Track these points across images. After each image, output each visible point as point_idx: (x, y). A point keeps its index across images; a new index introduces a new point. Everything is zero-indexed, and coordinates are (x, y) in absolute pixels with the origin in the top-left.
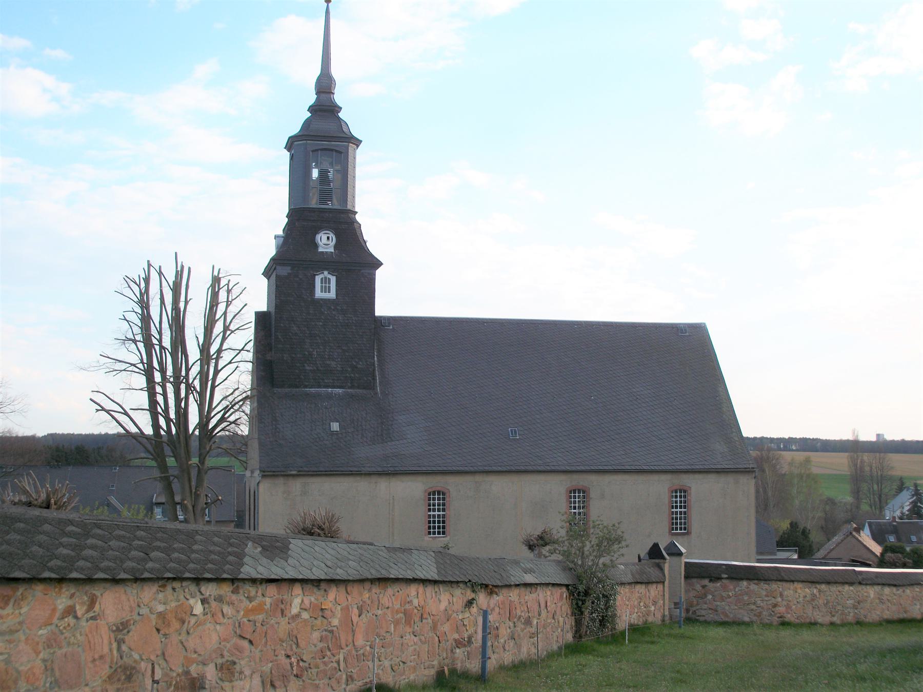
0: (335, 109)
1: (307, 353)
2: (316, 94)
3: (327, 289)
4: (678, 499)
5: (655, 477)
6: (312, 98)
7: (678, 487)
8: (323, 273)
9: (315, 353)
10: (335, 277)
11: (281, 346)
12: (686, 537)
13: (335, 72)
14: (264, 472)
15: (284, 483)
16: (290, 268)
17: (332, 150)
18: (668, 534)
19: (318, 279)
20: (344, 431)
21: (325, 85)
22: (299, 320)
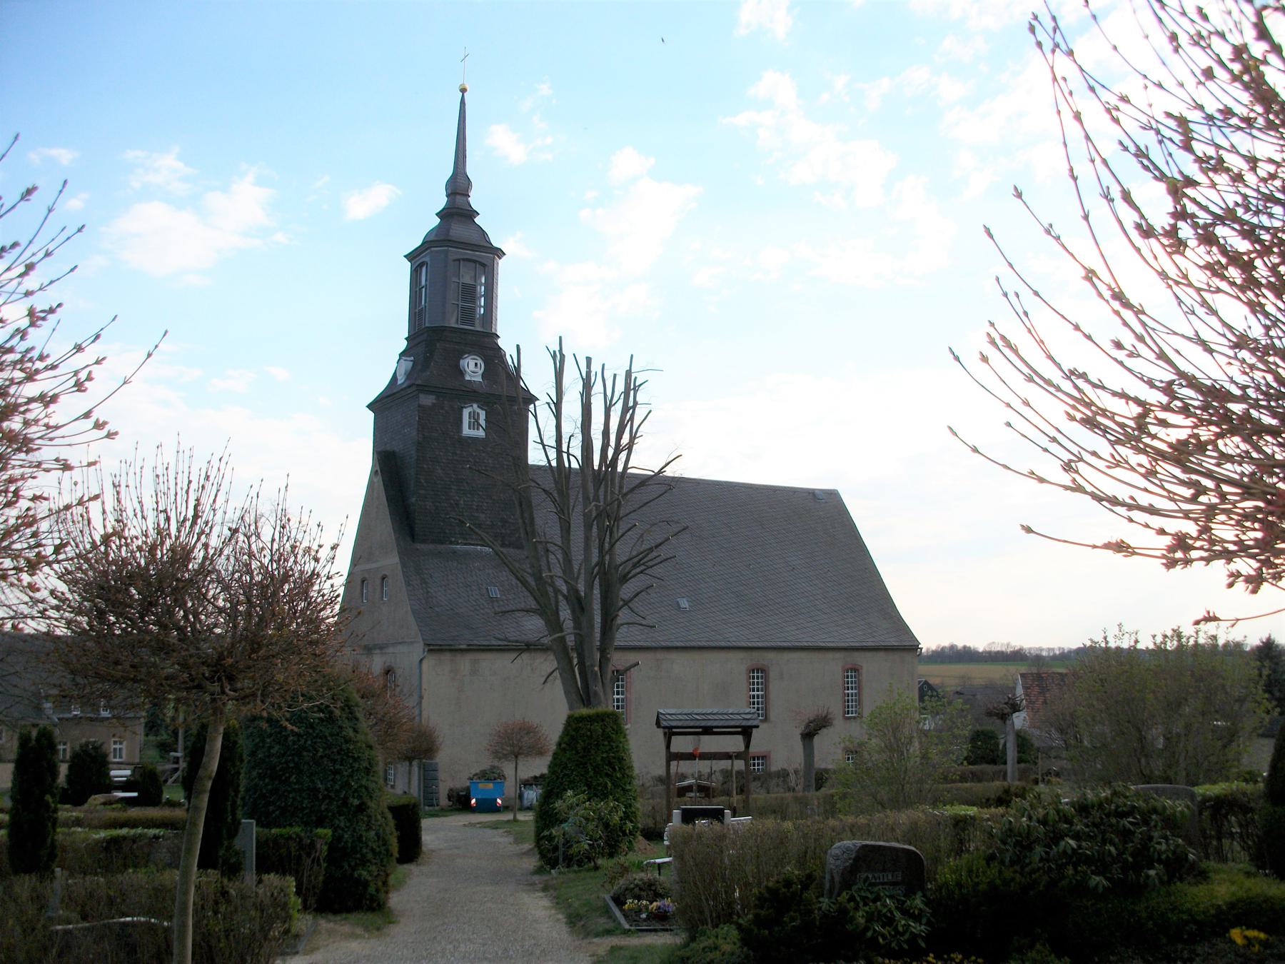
0: (471, 214)
2: (447, 196)
3: (475, 424)
4: (756, 680)
5: (830, 655)
6: (441, 201)
7: (850, 666)
8: (472, 406)
9: (462, 502)
10: (484, 412)
11: (422, 492)
14: (429, 645)
16: (434, 397)
17: (475, 261)
18: (841, 718)
19: (466, 413)
20: (504, 597)
21: (458, 187)
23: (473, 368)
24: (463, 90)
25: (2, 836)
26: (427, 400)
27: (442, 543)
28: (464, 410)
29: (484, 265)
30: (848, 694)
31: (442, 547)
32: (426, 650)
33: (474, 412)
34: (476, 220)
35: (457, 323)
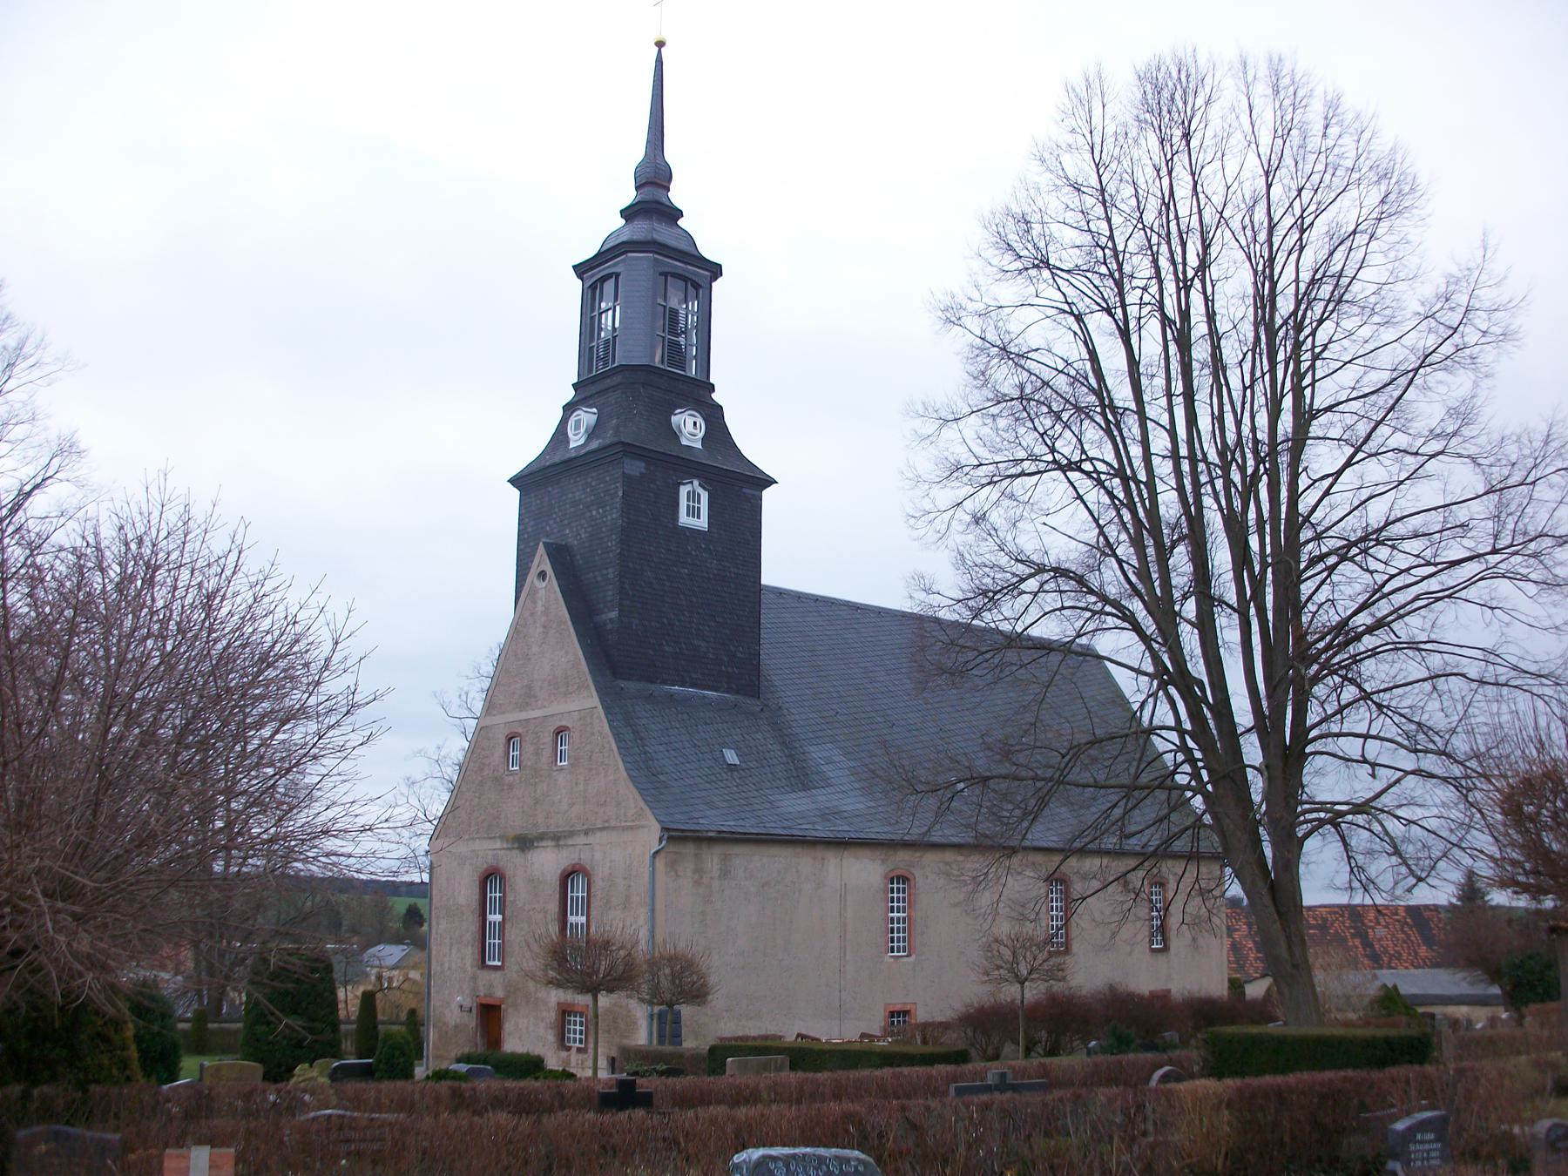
1: (665, 621)
6: (629, 195)
8: (692, 483)
12: (1165, 954)
13: (673, 154)
14: (668, 830)
15: (696, 855)
16: (643, 464)
19: (684, 491)
22: (655, 560)
23: (689, 427)
24: (660, 44)
25: (213, 1166)
26: (636, 467)
27: (652, 682)
28: (682, 488)
29: (697, 286)
30: (892, 919)
31: (653, 687)
32: (666, 837)
33: (694, 492)
34: (679, 223)
35: (662, 362)
